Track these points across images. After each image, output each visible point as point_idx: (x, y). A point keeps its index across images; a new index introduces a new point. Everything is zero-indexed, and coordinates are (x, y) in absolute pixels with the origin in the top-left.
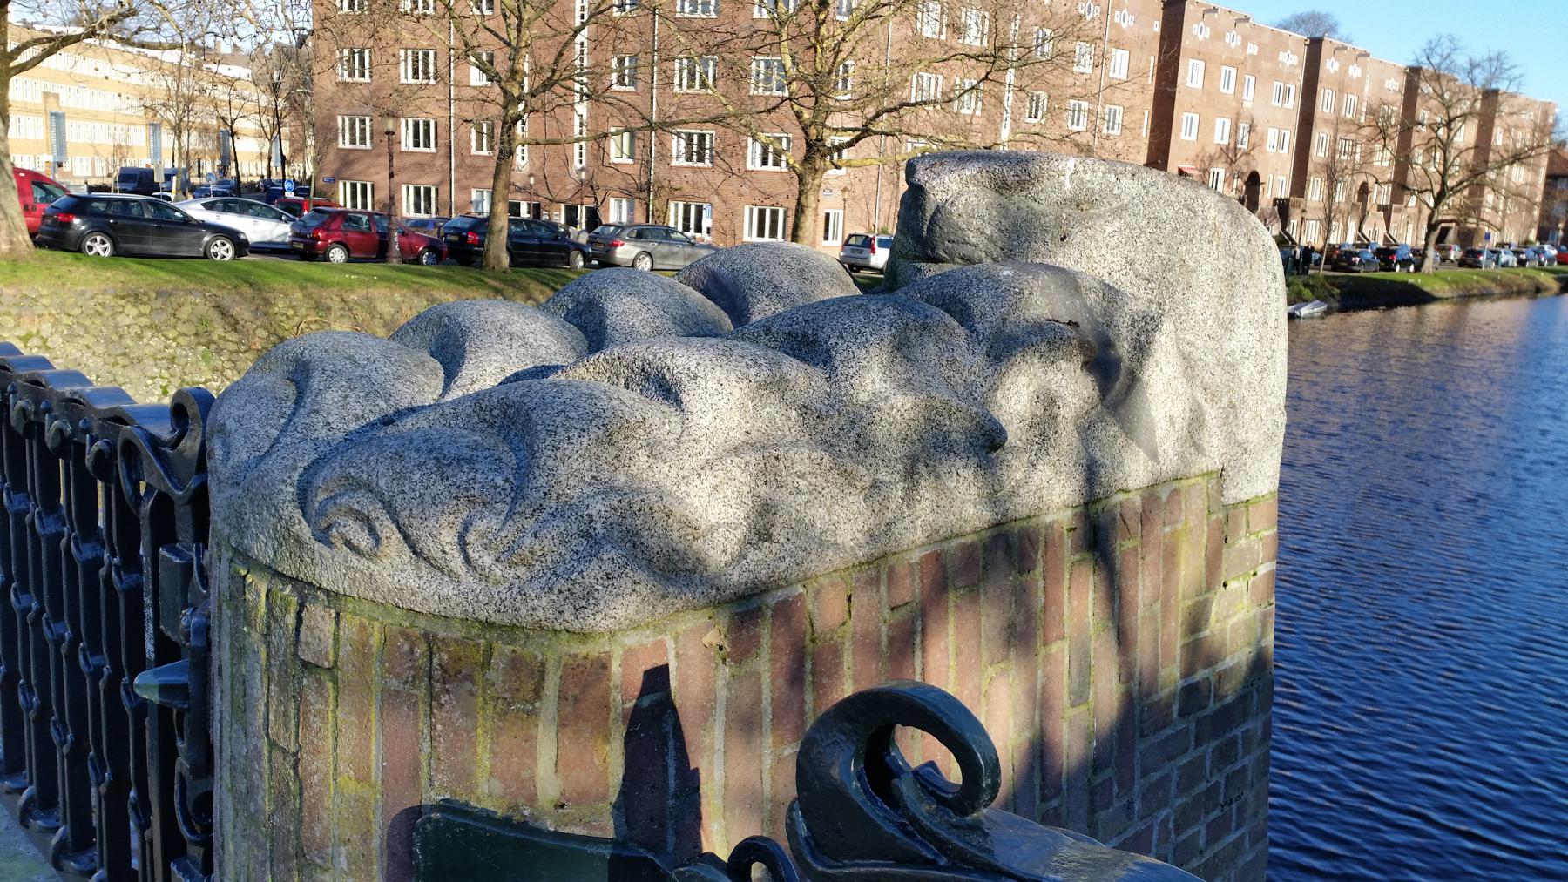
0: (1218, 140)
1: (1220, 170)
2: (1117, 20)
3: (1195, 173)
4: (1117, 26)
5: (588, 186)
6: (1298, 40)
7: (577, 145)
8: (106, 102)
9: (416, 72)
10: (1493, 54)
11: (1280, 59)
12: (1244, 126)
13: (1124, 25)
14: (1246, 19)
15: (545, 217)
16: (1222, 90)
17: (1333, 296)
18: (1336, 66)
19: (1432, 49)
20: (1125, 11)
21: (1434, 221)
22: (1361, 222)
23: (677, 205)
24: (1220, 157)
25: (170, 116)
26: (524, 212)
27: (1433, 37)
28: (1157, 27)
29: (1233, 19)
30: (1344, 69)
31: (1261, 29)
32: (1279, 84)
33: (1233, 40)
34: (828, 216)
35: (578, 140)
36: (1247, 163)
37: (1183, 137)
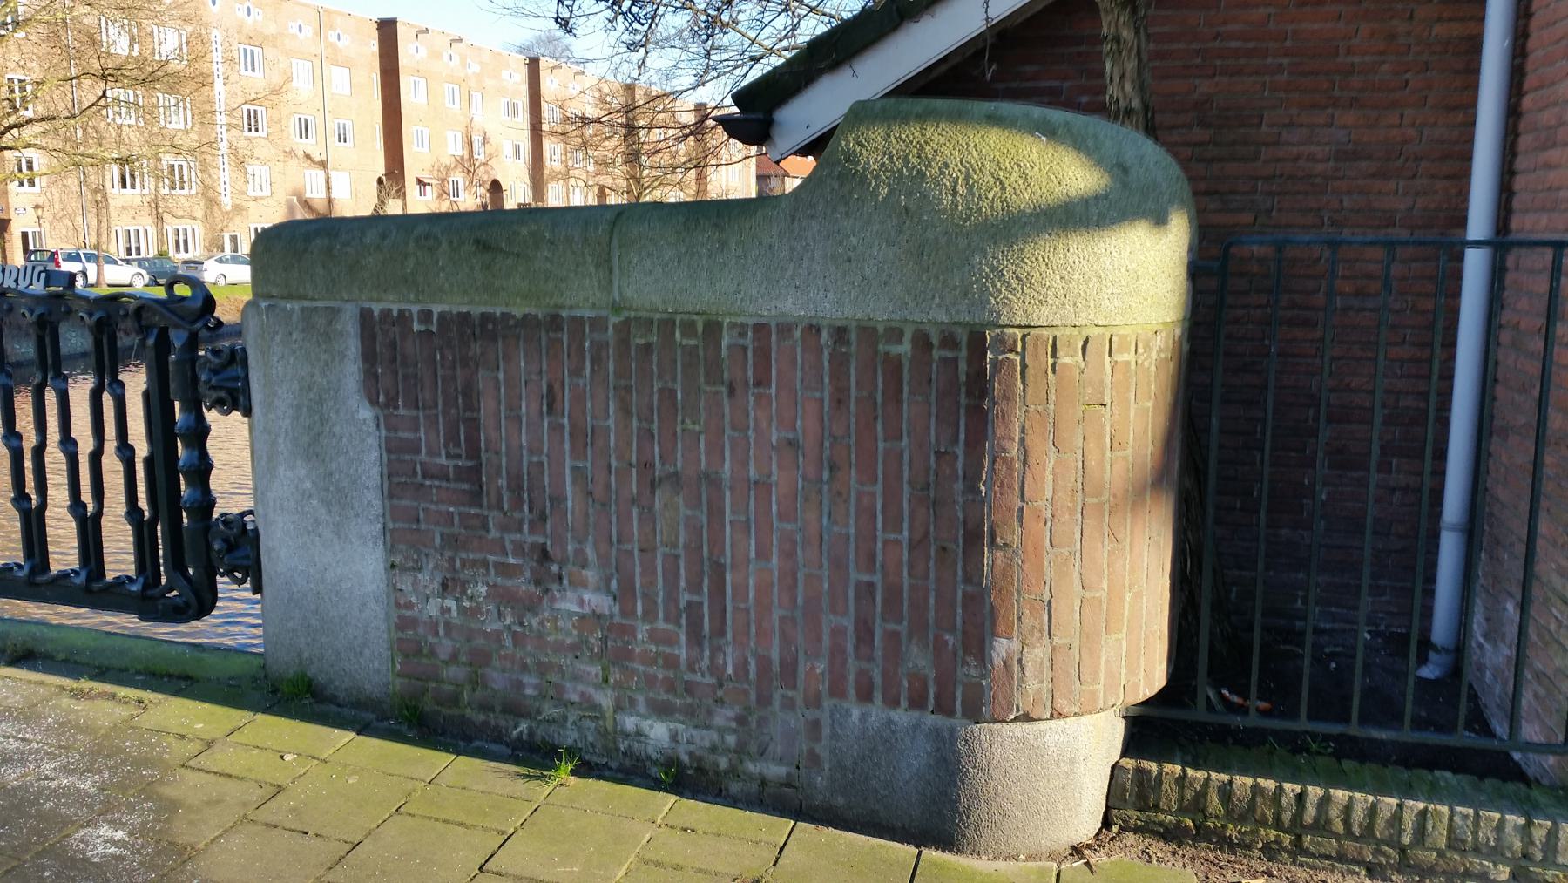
1: (458, 177)
3: (434, 182)
12: (477, 139)
13: (339, 44)
24: (456, 167)
36: (487, 172)
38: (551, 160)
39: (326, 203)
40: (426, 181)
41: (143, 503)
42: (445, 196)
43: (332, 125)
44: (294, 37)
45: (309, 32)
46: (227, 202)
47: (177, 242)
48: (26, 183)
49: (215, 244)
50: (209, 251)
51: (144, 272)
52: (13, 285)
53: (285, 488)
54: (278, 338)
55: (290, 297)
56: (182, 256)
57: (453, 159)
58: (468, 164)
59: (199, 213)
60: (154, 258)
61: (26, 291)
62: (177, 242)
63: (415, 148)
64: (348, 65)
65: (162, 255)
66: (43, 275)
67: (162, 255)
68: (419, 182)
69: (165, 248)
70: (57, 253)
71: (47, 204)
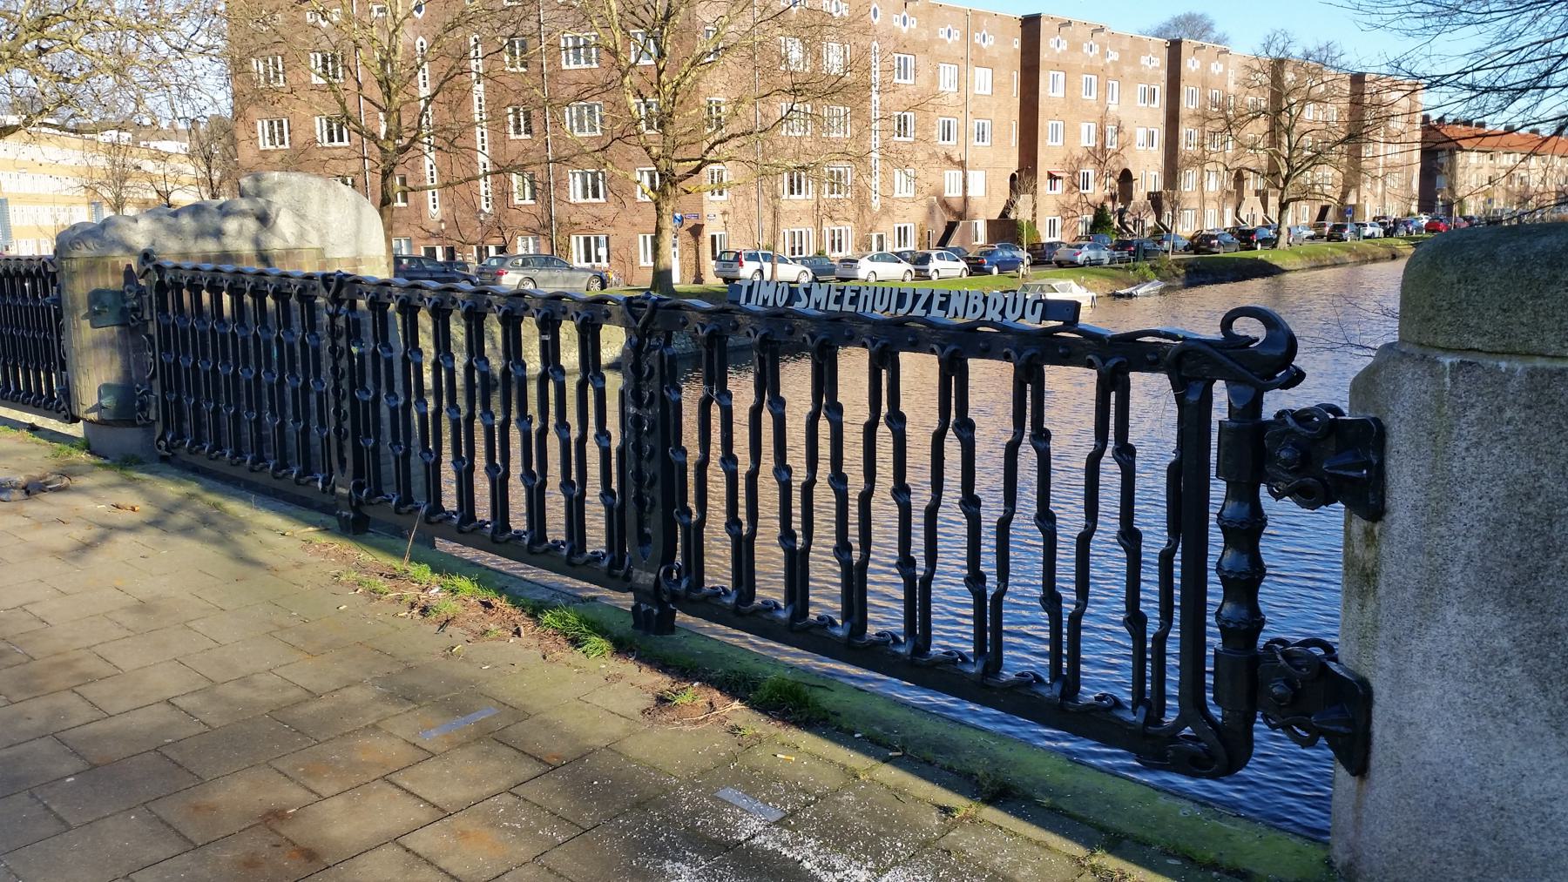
0: (1084, 143)
1: (1090, 170)
2: (977, 41)
3: (1065, 175)
4: (979, 48)
5: (498, 226)
6: (1158, 43)
7: (430, 192)
8: (45, 185)
9: (272, 136)
10: (1322, 45)
11: (1143, 62)
12: (1111, 128)
13: (984, 45)
14: (1102, 29)
15: (459, 258)
16: (1084, 97)
17: (1177, 276)
18: (1198, 64)
19: (1270, 44)
20: (984, 32)
21: (1284, 201)
22: (1237, 209)
23: (578, 238)
24: (1087, 159)
25: (107, 194)
26: (440, 257)
27: (1269, 32)
28: (1017, 45)
29: (1088, 30)
30: (1206, 67)
31: (1120, 36)
32: (1143, 86)
33: (1090, 50)
34: (713, 238)
35: (430, 188)
36: (1118, 162)
37: (1049, 142)
38: (1187, 143)
39: (962, 201)
40: (1057, 175)
41: (1150, 604)
42: (1075, 189)
43: (973, 125)
44: (944, 41)
45: (956, 36)
46: (876, 204)
47: (833, 242)
48: (717, 194)
49: (865, 244)
50: (860, 250)
51: (809, 270)
52: (998, 318)
53: (1455, 640)
54: (1472, 415)
55: (1510, 353)
56: (837, 254)
57: (1086, 151)
58: (1099, 155)
59: (852, 215)
60: (814, 257)
61: (1015, 326)
62: (833, 242)
63: (1049, 142)
64: (990, 64)
65: (820, 254)
66: (1040, 306)
67: (820, 254)
68: (1051, 176)
69: (822, 248)
70: (741, 253)
71: (731, 212)
